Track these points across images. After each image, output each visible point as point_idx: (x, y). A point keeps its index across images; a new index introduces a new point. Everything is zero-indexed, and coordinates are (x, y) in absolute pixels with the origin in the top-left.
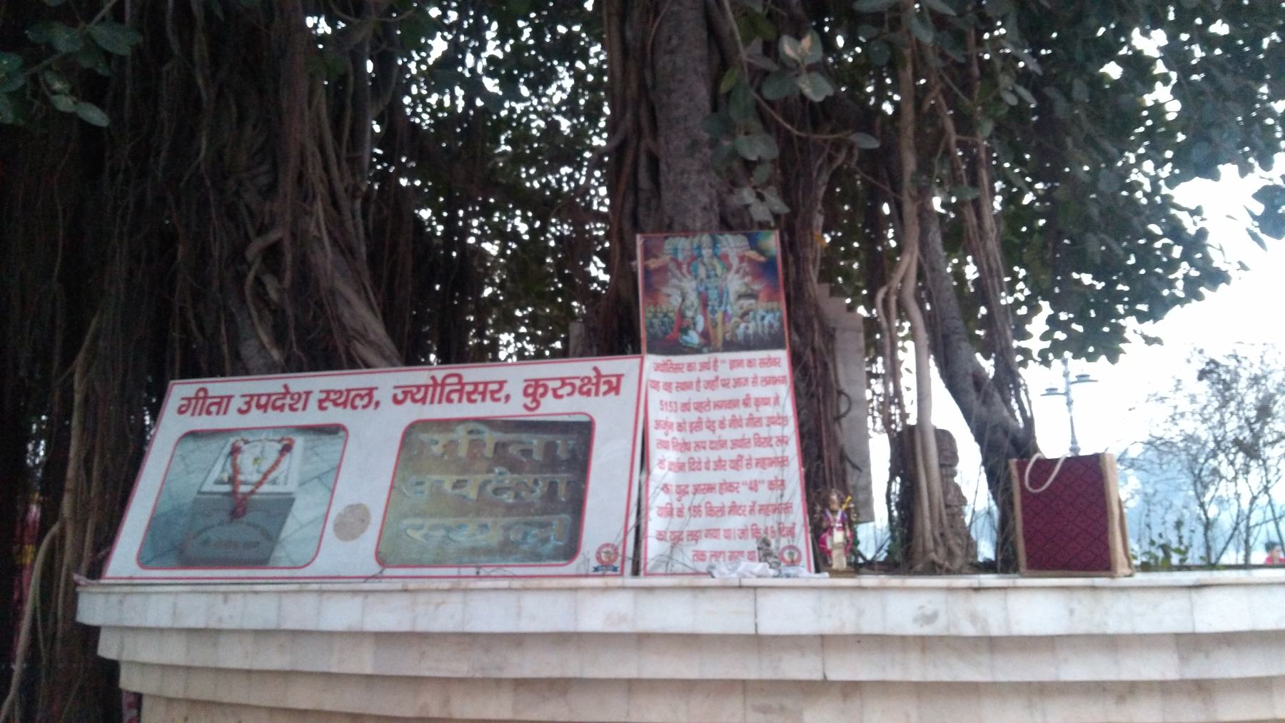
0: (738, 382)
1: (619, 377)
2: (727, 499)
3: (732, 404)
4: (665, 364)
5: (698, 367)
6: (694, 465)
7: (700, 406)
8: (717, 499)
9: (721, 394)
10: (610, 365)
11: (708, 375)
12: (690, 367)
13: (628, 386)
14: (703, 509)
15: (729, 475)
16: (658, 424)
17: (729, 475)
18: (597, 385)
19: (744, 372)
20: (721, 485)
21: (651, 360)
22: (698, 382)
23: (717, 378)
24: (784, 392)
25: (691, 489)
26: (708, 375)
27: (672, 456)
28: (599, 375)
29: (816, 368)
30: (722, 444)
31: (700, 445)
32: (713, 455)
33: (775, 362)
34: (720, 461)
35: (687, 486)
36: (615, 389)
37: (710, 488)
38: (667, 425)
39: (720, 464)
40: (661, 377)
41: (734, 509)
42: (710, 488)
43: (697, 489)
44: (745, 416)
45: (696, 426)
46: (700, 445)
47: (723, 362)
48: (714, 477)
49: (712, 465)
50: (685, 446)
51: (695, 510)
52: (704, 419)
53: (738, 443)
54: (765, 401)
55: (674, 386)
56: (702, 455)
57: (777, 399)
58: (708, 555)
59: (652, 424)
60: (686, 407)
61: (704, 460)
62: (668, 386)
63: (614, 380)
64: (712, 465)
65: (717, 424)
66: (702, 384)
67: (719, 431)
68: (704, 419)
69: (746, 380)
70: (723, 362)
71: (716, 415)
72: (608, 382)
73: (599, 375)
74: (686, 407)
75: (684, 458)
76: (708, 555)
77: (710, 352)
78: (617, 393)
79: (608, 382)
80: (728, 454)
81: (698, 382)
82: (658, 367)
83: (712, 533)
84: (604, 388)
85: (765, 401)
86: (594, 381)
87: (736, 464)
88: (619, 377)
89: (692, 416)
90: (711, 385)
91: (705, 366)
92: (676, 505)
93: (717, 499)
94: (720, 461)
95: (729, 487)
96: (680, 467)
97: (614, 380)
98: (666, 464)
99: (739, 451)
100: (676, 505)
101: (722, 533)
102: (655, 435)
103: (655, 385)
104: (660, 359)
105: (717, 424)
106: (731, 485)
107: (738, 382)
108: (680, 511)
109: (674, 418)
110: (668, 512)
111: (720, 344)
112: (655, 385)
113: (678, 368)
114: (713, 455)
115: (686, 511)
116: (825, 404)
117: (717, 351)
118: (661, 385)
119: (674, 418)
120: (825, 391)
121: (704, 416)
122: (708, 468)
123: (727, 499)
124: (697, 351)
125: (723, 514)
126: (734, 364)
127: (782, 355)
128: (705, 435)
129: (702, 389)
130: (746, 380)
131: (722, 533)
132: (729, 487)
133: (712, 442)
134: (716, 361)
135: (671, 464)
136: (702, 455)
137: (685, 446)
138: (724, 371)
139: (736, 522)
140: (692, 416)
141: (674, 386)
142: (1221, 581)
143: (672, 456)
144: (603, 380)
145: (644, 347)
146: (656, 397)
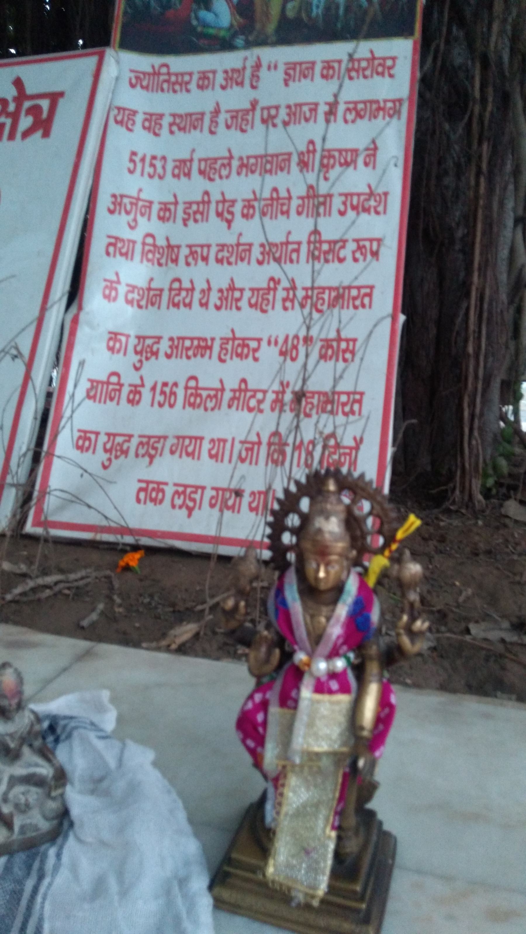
0: (297, 113)
1: (55, 98)
2: (230, 373)
3: (271, 163)
4: (156, 73)
5: (220, 79)
6: (178, 296)
7: (211, 168)
8: (211, 372)
9: (252, 142)
10: (43, 74)
11: (236, 98)
12: (205, 80)
13: (67, 120)
14: (180, 392)
15: (246, 322)
16: (118, 204)
17: (246, 322)
18: (15, 117)
19: (316, 91)
20: (225, 341)
21: (120, 64)
22: (217, 112)
23: (254, 104)
24: (393, 140)
25: (164, 346)
26: (236, 98)
27: (135, 272)
28: (22, 95)
29: (484, 100)
30: (240, 252)
31: (198, 254)
32: (219, 276)
33: (383, 67)
34: (232, 288)
35: (158, 339)
36: (43, 125)
37: (202, 347)
38: (139, 206)
39: (230, 297)
40: (138, 101)
41: (243, 396)
42: (202, 347)
43: (179, 347)
44: (299, 190)
45: (196, 212)
46: (198, 254)
47: (273, 67)
48: (212, 324)
49: (214, 298)
50: (168, 254)
51: (166, 394)
52: (216, 196)
53: (273, 252)
54: (348, 159)
55: (166, 121)
56: (197, 274)
57: (373, 150)
58: (169, 490)
59: (104, 201)
60: (183, 168)
61: (201, 285)
62: (153, 124)
63: (45, 104)
64: (214, 298)
65: (237, 209)
66: (222, 118)
67: (239, 222)
68: (216, 196)
69: (314, 108)
70: (273, 67)
71: (239, 187)
72: (35, 111)
73: (22, 95)
74: (183, 168)
75: (162, 279)
76: (169, 490)
77: (248, 45)
78: (46, 134)
79: (35, 111)
80: (251, 275)
81: (217, 112)
82: (138, 81)
83: (187, 446)
84: (26, 122)
85: (348, 159)
86: (12, 107)
87: (261, 300)
88: (55, 98)
89: (192, 188)
90: (240, 120)
91: (233, 78)
92: (130, 377)
93: (211, 372)
94: (232, 288)
95: (241, 347)
96: (149, 297)
97: (45, 104)
98: (122, 289)
99: (272, 269)
100: (130, 377)
101: (206, 446)
102: (106, 225)
103: (125, 117)
104: (144, 62)
105: (237, 209)
106: (244, 343)
107: (297, 113)
108: (136, 391)
109: (154, 191)
110: (105, 390)
111: (271, 28)
112: (125, 117)
113: (178, 83)
114: (219, 276)
115: (146, 394)
116: (490, 181)
117: (262, 42)
118: (139, 118)
119: (154, 191)
120: (494, 152)
121: (216, 189)
122: (204, 305)
123: (230, 373)
124: (225, 45)
125: (218, 406)
126: (295, 72)
127: (401, 50)
128: (211, 231)
129: (221, 128)
130: (314, 108)
131: (206, 446)
132: (241, 347)
133: (222, 247)
134: (258, 66)
135: (133, 288)
136: (197, 274)
137: (168, 254)
138: (272, 90)
139: (234, 425)
140: (192, 188)
141: (166, 121)
142: (54, 349)
143: (135, 272)
144: (27, 104)
145: (116, 35)
146: (123, 142)
